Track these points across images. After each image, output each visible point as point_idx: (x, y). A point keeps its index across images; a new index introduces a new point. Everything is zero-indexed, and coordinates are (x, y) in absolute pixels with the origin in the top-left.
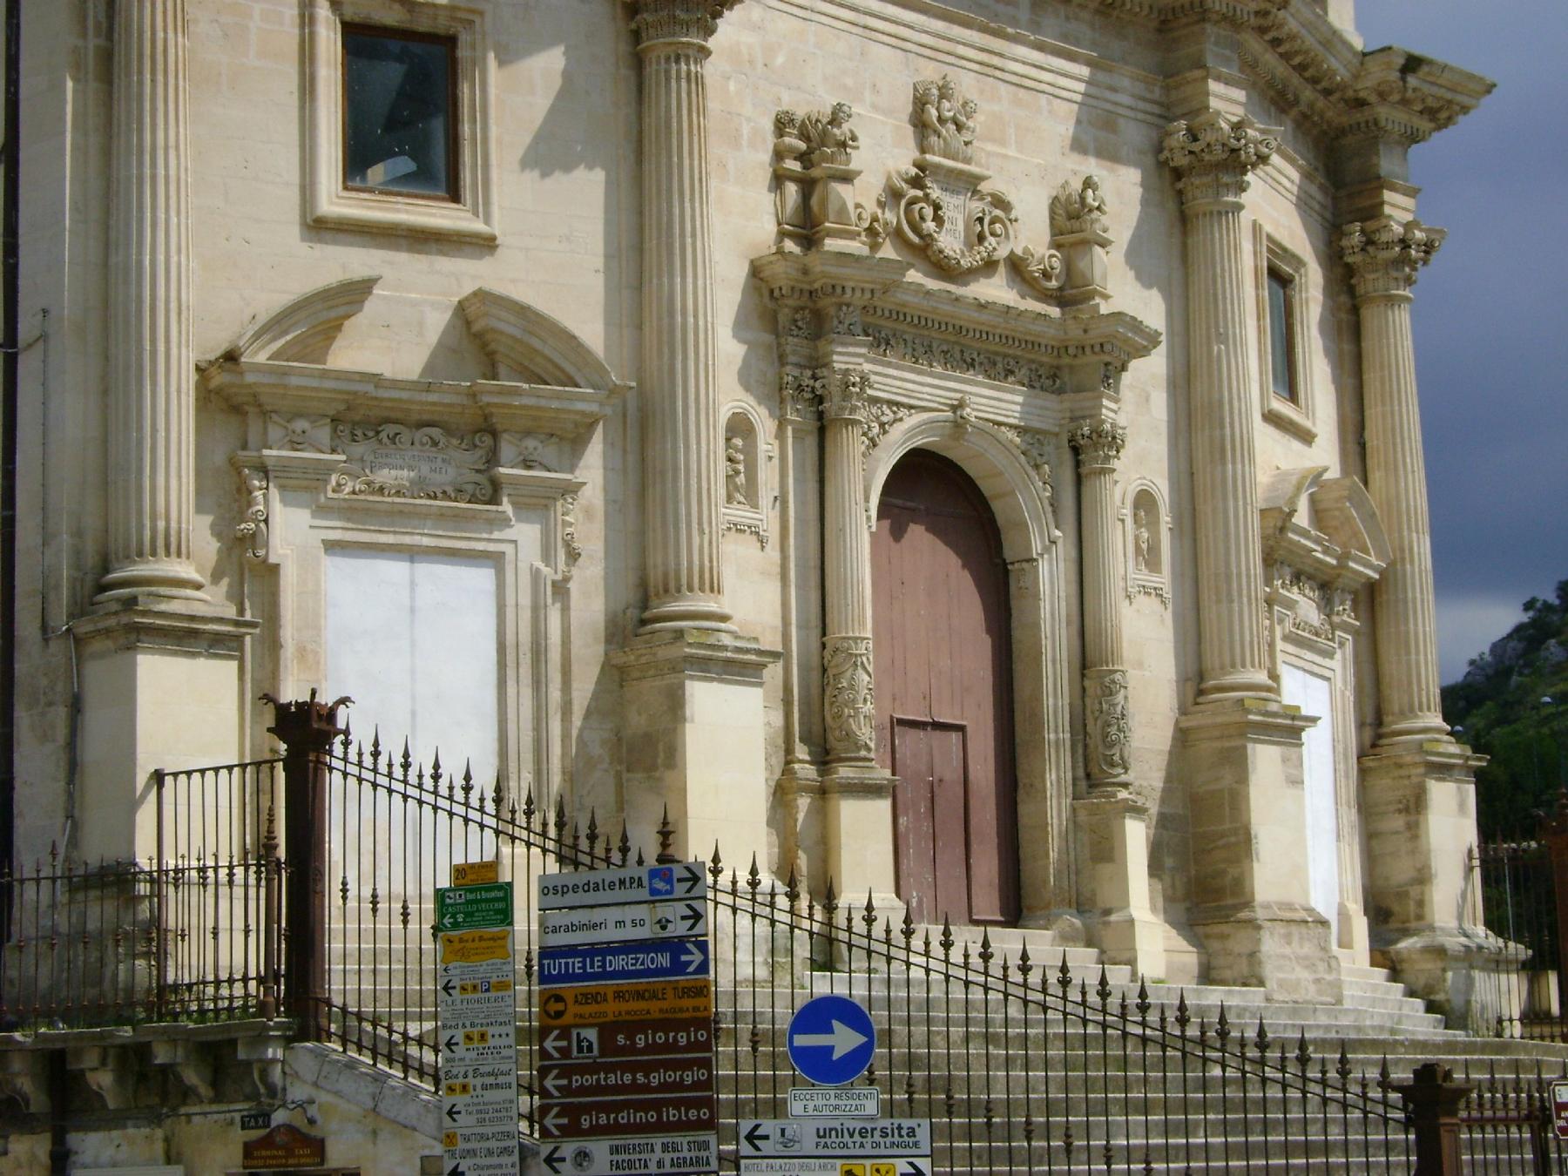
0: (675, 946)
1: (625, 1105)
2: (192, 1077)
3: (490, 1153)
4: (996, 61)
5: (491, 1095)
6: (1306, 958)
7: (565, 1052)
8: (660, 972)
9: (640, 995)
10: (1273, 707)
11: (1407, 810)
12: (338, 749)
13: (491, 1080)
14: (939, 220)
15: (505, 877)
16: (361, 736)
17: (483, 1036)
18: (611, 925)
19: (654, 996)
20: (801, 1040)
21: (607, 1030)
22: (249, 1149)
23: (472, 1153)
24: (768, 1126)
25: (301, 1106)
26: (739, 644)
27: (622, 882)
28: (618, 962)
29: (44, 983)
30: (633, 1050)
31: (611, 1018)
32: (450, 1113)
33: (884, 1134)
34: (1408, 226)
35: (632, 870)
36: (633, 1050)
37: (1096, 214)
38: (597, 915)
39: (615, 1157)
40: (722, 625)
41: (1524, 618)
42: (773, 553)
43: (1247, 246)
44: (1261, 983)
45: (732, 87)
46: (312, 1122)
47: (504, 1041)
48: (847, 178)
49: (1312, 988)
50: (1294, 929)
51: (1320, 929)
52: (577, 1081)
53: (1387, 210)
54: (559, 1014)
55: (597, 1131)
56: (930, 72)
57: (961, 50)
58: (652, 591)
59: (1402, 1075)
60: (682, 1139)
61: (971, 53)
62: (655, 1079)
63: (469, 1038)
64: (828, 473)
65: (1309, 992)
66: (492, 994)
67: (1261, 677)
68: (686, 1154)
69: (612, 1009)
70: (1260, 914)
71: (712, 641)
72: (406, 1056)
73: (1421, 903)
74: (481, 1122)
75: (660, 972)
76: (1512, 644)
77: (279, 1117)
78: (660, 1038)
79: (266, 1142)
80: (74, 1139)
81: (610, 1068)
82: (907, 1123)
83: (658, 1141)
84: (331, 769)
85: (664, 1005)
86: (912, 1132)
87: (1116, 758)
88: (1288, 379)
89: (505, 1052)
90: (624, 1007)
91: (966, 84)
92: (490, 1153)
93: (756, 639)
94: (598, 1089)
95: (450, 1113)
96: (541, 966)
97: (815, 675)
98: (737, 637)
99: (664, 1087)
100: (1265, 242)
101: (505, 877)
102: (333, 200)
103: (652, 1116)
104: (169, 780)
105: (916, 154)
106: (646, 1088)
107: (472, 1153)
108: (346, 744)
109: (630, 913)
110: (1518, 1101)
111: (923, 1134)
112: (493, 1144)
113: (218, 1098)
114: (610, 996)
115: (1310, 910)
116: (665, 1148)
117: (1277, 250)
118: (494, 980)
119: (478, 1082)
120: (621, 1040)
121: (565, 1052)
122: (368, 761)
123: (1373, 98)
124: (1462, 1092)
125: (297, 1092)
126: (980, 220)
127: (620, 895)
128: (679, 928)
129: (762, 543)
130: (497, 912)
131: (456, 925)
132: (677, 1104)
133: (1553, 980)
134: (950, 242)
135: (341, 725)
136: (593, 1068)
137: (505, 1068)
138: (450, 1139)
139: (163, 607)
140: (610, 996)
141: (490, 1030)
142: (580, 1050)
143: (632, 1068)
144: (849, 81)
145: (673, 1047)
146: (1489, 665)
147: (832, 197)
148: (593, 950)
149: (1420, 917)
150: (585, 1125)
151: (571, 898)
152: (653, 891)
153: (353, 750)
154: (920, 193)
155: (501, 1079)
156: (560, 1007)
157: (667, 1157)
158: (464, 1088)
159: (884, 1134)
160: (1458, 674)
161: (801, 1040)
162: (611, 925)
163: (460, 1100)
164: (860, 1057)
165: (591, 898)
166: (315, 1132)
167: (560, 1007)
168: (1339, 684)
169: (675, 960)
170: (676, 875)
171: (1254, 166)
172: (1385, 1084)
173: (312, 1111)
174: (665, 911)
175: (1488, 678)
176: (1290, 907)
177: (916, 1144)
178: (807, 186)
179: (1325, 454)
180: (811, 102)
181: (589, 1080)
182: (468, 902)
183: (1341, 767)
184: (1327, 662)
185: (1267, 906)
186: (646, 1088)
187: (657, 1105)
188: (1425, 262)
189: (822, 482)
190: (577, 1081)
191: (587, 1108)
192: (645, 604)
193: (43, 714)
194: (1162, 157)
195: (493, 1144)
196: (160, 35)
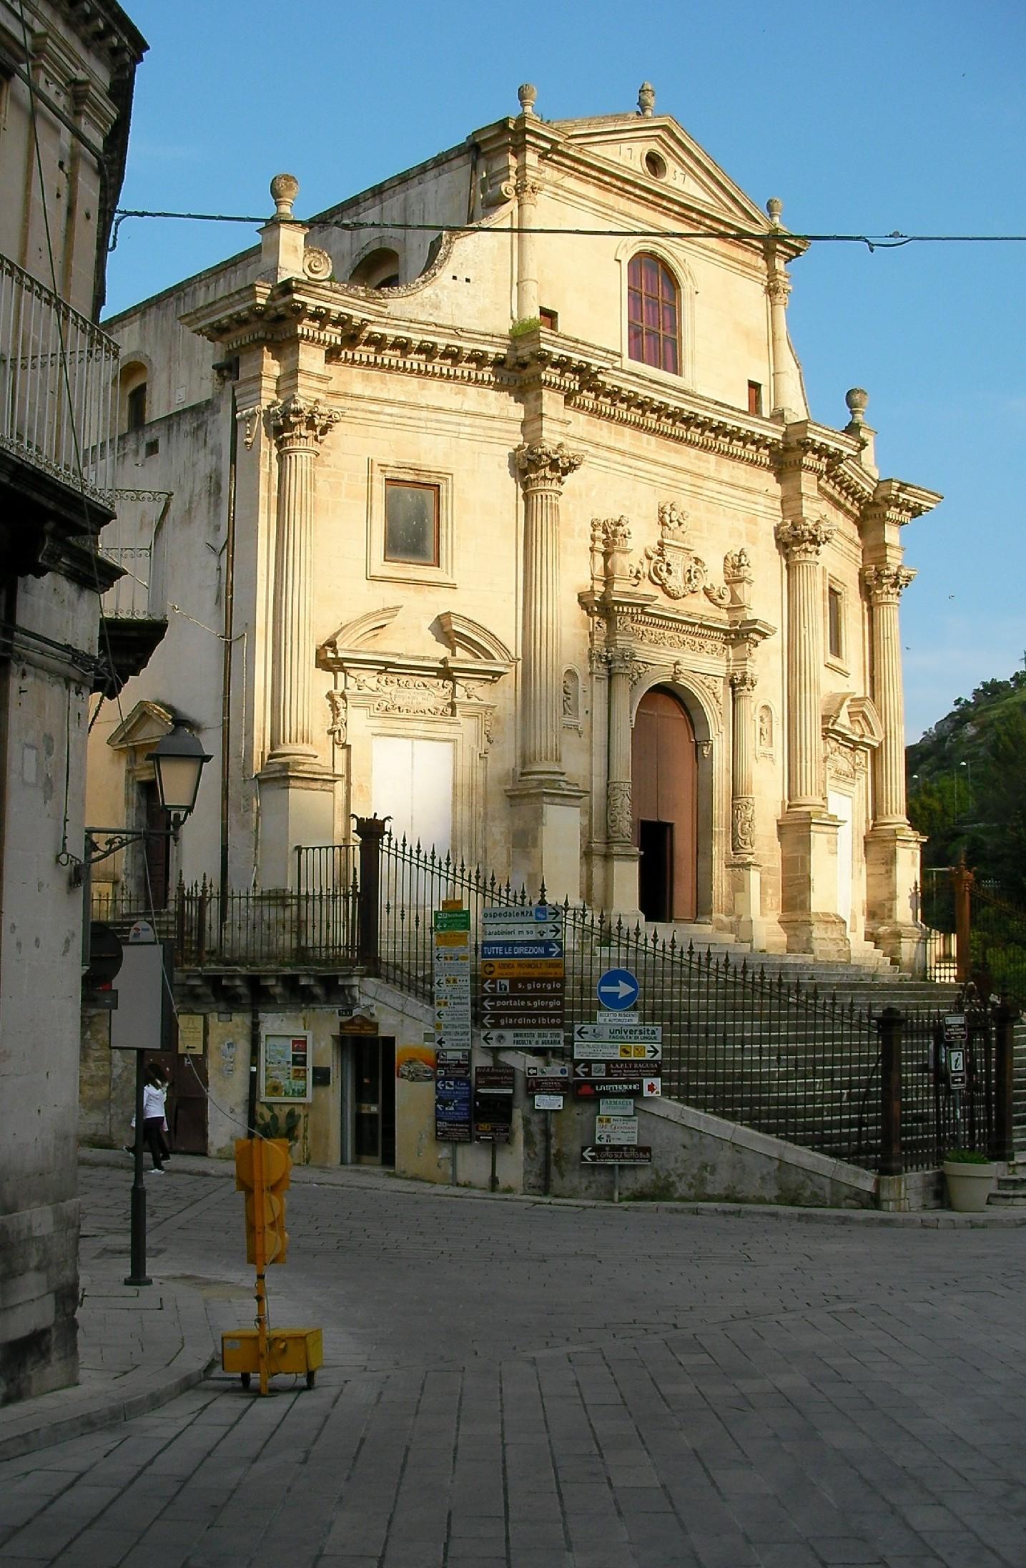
0: (547, 944)
1: (518, 1016)
2: (318, 991)
3: (457, 1033)
4: (699, 490)
5: (458, 1007)
6: (834, 939)
7: (494, 990)
8: (539, 955)
9: (529, 966)
10: (825, 816)
11: (886, 863)
12: (386, 842)
13: (459, 1001)
14: (669, 572)
15: (465, 908)
16: (397, 837)
17: (455, 981)
18: (516, 932)
19: (536, 966)
20: (604, 989)
21: (514, 982)
22: (342, 1025)
23: (449, 1033)
24: (587, 1028)
25: (368, 1007)
26: (569, 787)
27: (523, 913)
28: (520, 950)
29: (243, 942)
30: (525, 990)
31: (515, 976)
32: (438, 1014)
33: (641, 1033)
34: (899, 567)
35: (527, 908)
36: (525, 990)
37: (746, 567)
38: (510, 928)
39: (516, 1039)
40: (562, 778)
41: (955, 709)
42: (585, 740)
43: (819, 579)
44: (812, 952)
45: (571, 507)
46: (372, 1015)
47: (464, 983)
48: (625, 552)
49: (836, 955)
50: (829, 925)
51: (842, 926)
52: (499, 1004)
53: (888, 559)
54: (491, 973)
55: (507, 1026)
56: (666, 497)
57: (681, 485)
58: (527, 760)
59: (878, 1012)
60: (548, 1032)
61: (687, 487)
62: (535, 1004)
63: (448, 981)
64: (613, 700)
65: (835, 957)
66: (460, 962)
67: (819, 801)
68: (549, 1039)
69: (517, 972)
70: (813, 918)
71: (557, 786)
72: (416, 986)
73: (891, 910)
74: (453, 1019)
75: (539, 955)
76: (948, 723)
77: (356, 1012)
78: (539, 986)
79: (351, 1022)
80: (262, 1015)
81: (514, 998)
82: (651, 1028)
83: (536, 1032)
84: (382, 851)
85: (540, 971)
86: (653, 1032)
87: (748, 841)
88: (836, 648)
89: (465, 988)
90: (522, 971)
91: (684, 502)
92: (457, 1033)
93: (577, 785)
94: (508, 1008)
95: (438, 1014)
96: (483, 951)
97: (604, 800)
98: (568, 784)
99: (539, 1008)
100: (377, 469)
101: (465, 908)
102: (380, 566)
103: (534, 1021)
104: (304, 851)
105: (660, 538)
106: (531, 1008)
107: (449, 1033)
108: (390, 839)
109: (526, 928)
110: (929, 1023)
111: (659, 1034)
112: (459, 1030)
113: (327, 1002)
114: (516, 965)
115: (837, 916)
116: (539, 1035)
117: (833, 579)
118: (461, 955)
119: (452, 1001)
120: (520, 986)
121: (494, 990)
122: (400, 848)
123: (882, 503)
124: (903, 1021)
125: (365, 1001)
126: (689, 571)
127: (520, 919)
128: (549, 936)
129: (580, 734)
130: (463, 924)
131: (442, 929)
132: (545, 1016)
133: (954, 938)
134: (675, 582)
135: (387, 829)
136: (506, 998)
137: (465, 995)
138: (438, 1026)
139: (305, 768)
140: (516, 965)
141: (458, 978)
142: (501, 989)
143: (526, 998)
144: (627, 503)
145: (545, 990)
146: (934, 735)
147: (618, 562)
148: (505, 944)
149: (890, 917)
150: (503, 1023)
151: (498, 920)
152: (537, 918)
153: (393, 843)
154: (660, 558)
155: (463, 1001)
156: (492, 969)
157: (541, 1040)
158: (446, 1004)
159: (641, 1033)
160: (916, 740)
161: (604, 989)
162: (516, 932)
163: (443, 1008)
164: (631, 996)
165: (507, 920)
166: (374, 1020)
167: (492, 969)
168: (857, 800)
169: (546, 950)
170: (548, 911)
171: (824, 543)
172: (870, 1016)
173: (373, 1010)
174: (541, 927)
175: (934, 742)
176: (827, 914)
177: (655, 1038)
178: (607, 555)
179: (856, 685)
180: (609, 513)
181: (505, 1003)
182: (449, 919)
183: (856, 841)
184: (851, 788)
185: (817, 914)
186: (531, 1008)
187: (536, 1016)
188: (907, 585)
189: (609, 703)
190: (499, 1004)
191: (503, 1016)
192: (524, 765)
193: (243, 815)
194: (778, 537)
195: (459, 1030)
196: (304, 492)
